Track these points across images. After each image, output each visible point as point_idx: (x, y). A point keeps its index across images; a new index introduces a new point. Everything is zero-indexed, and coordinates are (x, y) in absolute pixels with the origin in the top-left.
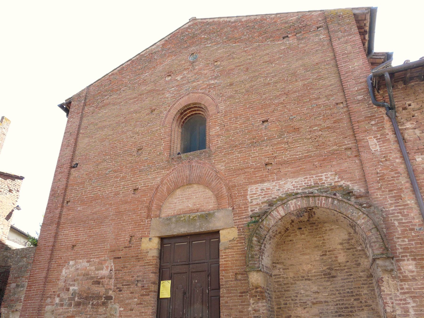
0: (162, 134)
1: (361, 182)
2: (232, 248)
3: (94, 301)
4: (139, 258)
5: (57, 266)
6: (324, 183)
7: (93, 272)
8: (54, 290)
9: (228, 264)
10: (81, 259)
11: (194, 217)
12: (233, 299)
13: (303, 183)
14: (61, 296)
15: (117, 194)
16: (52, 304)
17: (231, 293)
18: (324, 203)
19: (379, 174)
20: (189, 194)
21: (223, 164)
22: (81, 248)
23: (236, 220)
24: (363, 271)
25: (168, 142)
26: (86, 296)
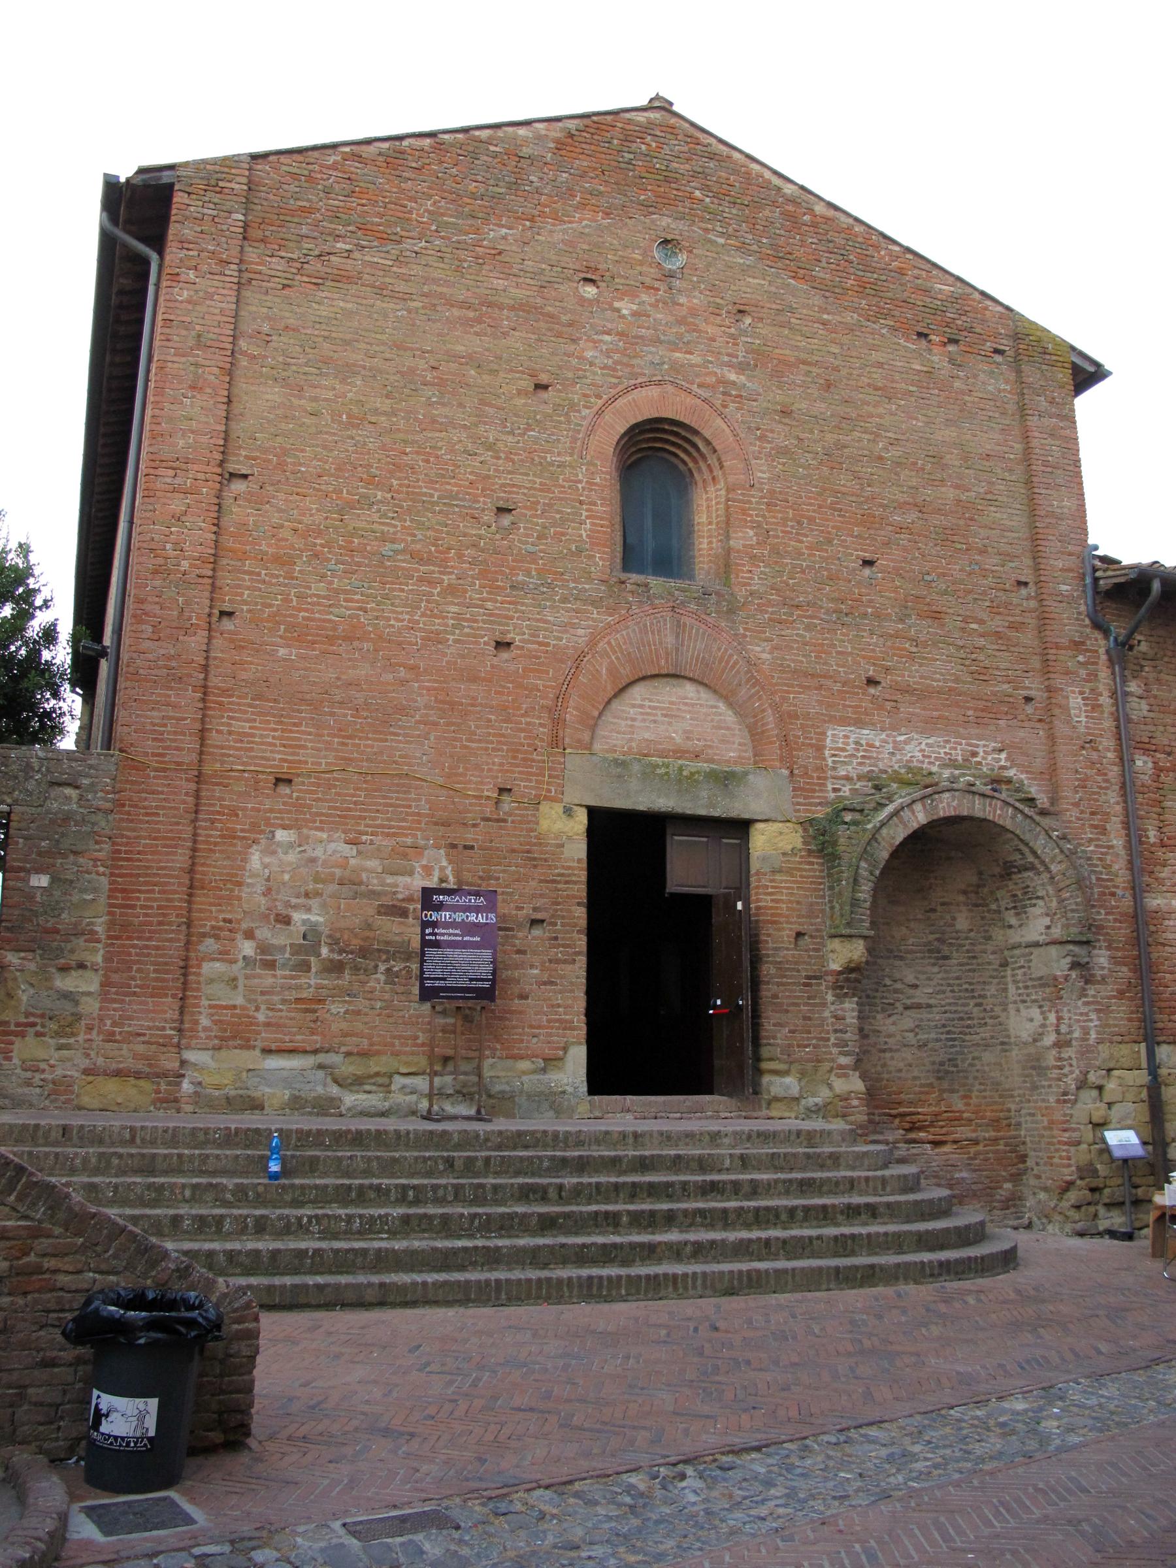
0: (580, 486)
1: (1043, 780)
2: (789, 872)
3: (392, 963)
4: (535, 859)
5: (222, 836)
6: (980, 763)
7: (377, 878)
8: (228, 916)
9: (781, 909)
10: (321, 829)
11: (692, 774)
12: (791, 991)
13: (942, 751)
14: (258, 933)
15: (435, 638)
16: (225, 956)
17: (785, 976)
18: (1000, 816)
19: (1079, 773)
20: (672, 703)
21: (767, 646)
22: (315, 792)
23: (798, 804)
24: (994, 953)
25: (602, 519)
26: (361, 947)
